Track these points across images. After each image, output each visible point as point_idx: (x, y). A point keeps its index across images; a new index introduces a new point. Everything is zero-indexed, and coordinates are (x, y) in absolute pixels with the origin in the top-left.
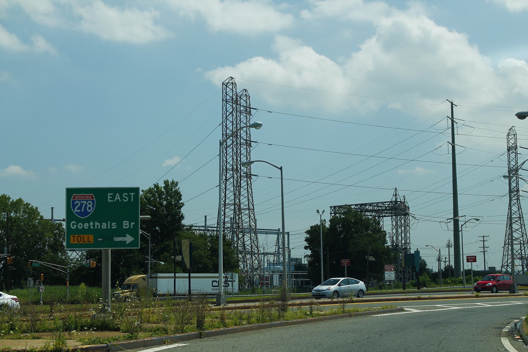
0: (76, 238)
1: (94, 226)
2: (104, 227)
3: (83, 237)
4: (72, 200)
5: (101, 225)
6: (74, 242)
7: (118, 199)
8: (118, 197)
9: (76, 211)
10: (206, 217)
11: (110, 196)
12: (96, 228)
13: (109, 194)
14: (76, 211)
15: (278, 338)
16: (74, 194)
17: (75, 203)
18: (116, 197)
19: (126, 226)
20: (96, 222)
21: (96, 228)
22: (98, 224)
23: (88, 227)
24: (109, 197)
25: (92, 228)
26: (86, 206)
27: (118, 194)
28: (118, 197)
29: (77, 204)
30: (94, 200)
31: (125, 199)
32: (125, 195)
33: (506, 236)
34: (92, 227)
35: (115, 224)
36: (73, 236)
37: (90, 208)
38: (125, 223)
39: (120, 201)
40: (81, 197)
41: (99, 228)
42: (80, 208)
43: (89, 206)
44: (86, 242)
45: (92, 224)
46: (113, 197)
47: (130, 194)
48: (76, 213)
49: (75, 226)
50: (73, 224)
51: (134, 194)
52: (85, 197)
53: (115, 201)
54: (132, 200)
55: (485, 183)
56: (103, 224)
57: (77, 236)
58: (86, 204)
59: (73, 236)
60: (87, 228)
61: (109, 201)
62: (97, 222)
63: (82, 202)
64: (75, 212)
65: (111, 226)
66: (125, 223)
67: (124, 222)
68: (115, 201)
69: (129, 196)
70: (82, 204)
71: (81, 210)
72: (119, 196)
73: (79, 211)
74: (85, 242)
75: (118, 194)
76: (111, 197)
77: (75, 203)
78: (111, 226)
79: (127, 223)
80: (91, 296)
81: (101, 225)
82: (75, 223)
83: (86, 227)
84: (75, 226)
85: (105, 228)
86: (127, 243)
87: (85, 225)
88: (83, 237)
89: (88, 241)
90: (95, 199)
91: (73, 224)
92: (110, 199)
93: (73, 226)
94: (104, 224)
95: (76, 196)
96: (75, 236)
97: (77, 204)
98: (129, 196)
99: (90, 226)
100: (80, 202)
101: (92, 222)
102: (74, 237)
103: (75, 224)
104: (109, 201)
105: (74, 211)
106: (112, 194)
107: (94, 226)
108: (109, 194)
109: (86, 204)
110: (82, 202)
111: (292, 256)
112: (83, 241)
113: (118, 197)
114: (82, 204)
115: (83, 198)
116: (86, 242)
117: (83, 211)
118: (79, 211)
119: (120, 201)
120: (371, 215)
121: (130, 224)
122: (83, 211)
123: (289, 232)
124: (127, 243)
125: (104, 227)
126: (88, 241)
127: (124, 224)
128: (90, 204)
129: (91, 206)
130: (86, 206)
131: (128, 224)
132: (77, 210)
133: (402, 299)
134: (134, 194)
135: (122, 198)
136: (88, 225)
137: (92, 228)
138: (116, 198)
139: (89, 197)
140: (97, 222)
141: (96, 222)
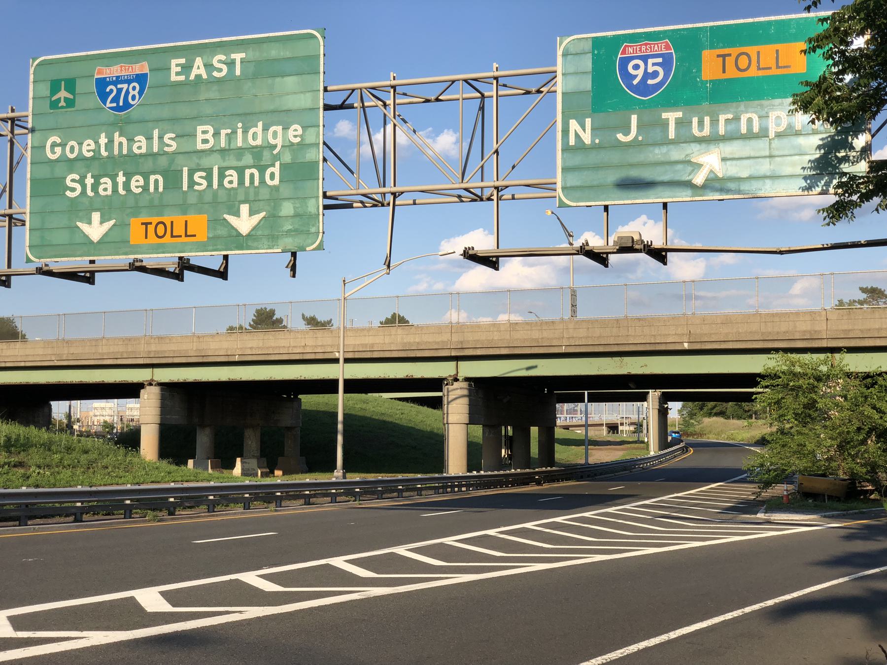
0: (730, 61)
3: (758, 53)
4: (619, 56)
5: (131, 140)
6: (724, 71)
8: (198, 68)
9: (109, 105)
11: (177, 65)
12: (116, 152)
13: (174, 62)
15: (832, 421)
17: (108, 90)
19: (205, 141)
20: (117, 134)
22: (124, 140)
25: (104, 153)
26: (127, 92)
28: (198, 68)
29: (112, 91)
30: (672, 53)
35: (173, 135)
36: (718, 56)
37: (134, 98)
39: (205, 76)
40: (641, 48)
41: (125, 152)
42: (116, 99)
43: (132, 93)
44: (770, 68)
46: (186, 68)
52: (651, 48)
53: (192, 77)
57: (734, 51)
58: (128, 89)
59: (718, 56)
62: (120, 136)
64: (108, 108)
67: (200, 129)
68: (192, 77)
69: (231, 64)
70: (119, 91)
71: (118, 103)
72: (202, 67)
73: (114, 105)
74: (763, 69)
76: (179, 69)
81: (131, 140)
82: (58, 141)
84: (58, 150)
87: (85, 148)
88: (758, 53)
89: (778, 67)
91: (54, 145)
92: (177, 74)
93: (53, 152)
96: (730, 55)
97: (112, 91)
98: (231, 64)
102: (724, 56)
103: (59, 145)
105: (106, 106)
106: (183, 61)
108: (174, 62)
109: (128, 89)
110: (119, 86)
112: (759, 68)
114: (119, 91)
115: (646, 49)
116: (770, 68)
117: (121, 104)
118: (114, 105)
119: (205, 76)
121: (216, 134)
122: (121, 104)
123: (514, 194)
126: (778, 67)
127: (200, 137)
128: (134, 88)
129: (136, 93)
130: (127, 92)
131: (209, 136)
133: (417, 509)
135: (209, 66)
137: (104, 153)
138: (195, 72)
139: (658, 47)
140: (120, 136)
141: (117, 134)
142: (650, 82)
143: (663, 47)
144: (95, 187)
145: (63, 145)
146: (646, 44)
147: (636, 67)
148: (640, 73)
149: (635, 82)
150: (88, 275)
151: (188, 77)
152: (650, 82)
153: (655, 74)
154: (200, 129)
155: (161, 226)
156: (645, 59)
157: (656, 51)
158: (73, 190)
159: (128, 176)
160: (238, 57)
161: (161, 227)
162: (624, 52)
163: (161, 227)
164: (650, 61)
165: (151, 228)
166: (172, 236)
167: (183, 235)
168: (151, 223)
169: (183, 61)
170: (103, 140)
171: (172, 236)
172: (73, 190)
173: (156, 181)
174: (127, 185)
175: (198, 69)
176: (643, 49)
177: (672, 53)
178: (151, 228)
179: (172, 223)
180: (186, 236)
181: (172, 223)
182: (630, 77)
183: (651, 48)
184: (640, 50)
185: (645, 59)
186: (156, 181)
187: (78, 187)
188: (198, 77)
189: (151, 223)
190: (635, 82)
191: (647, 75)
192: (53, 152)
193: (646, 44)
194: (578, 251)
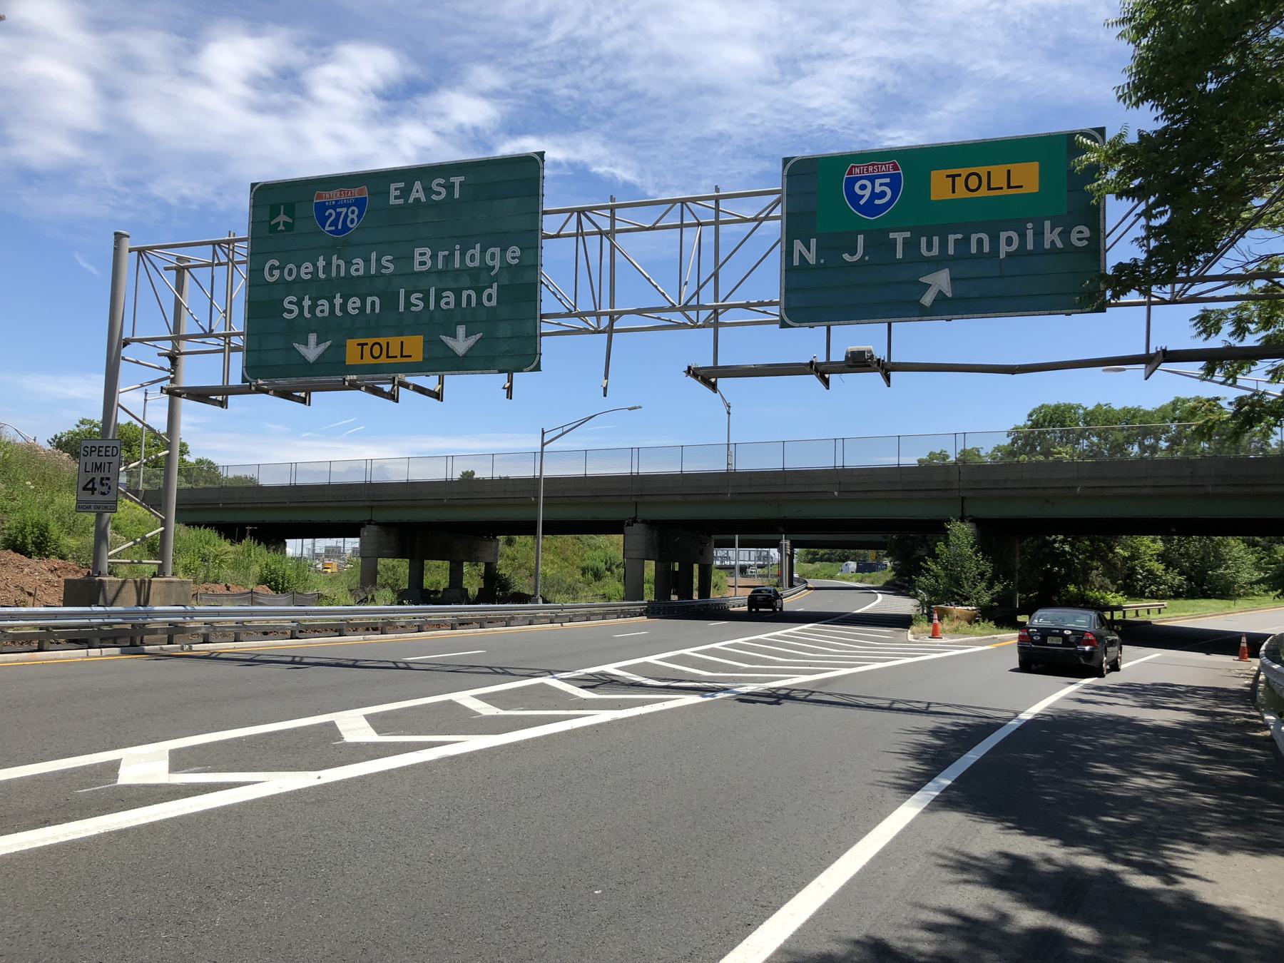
4: (846, 176)
5: (349, 263)
7: (417, 195)
8: (417, 192)
11: (396, 189)
13: (393, 186)
14: (326, 229)
16: (895, 161)
17: (327, 214)
18: (414, 190)
23: (1086, 239)
24: (393, 193)
25: (322, 276)
26: (346, 215)
27: (418, 185)
28: (417, 192)
29: (331, 214)
30: (900, 173)
34: (323, 274)
38: (421, 254)
39: (423, 199)
40: (868, 169)
41: (342, 274)
42: (335, 223)
43: (351, 216)
46: (405, 192)
47: (452, 180)
49: (277, 273)
50: (272, 268)
51: (462, 178)
52: (878, 168)
53: (411, 201)
54: (457, 196)
60: (1085, 243)
61: (392, 201)
63: (338, 210)
66: (421, 254)
67: (417, 251)
68: (411, 201)
69: (450, 187)
70: (339, 214)
71: (337, 227)
72: (421, 190)
73: (333, 228)
76: (398, 193)
79: (425, 254)
80: (1050, 429)
82: (277, 263)
84: (277, 273)
85: (361, 272)
87: (303, 270)
90: (901, 171)
91: (272, 268)
92: (396, 198)
95: (855, 167)
97: (331, 214)
98: (450, 187)
100: (335, 211)
104: (392, 201)
106: (402, 185)
108: (393, 186)
109: (347, 213)
110: (338, 210)
111: (118, 422)
113: (418, 192)
114: (339, 214)
115: (873, 169)
117: (340, 227)
118: (333, 228)
119: (423, 199)
120: (1208, 171)
121: (434, 257)
122: (340, 227)
127: (417, 259)
128: (353, 212)
130: (346, 215)
131: (427, 258)
132: (864, 195)
135: (428, 190)
137: (322, 276)
139: (886, 167)
142: (877, 202)
143: (891, 167)
145: (281, 268)
146: (873, 165)
147: (863, 187)
148: (867, 193)
149: (862, 202)
151: (406, 201)
152: (877, 202)
153: (883, 194)
154: (417, 251)
156: (872, 179)
157: (884, 171)
160: (457, 180)
162: (850, 173)
164: (878, 182)
169: (402, 185)
172: (291, 312)
174: (344, 307)
176: (870, 169)
177: (900, 173)
182: (855, 199)
184: (867, 171)
185: (872, 179)
188: (417, 200)
190: (862, 202)
191: (874, 196)
193: (873, 165)
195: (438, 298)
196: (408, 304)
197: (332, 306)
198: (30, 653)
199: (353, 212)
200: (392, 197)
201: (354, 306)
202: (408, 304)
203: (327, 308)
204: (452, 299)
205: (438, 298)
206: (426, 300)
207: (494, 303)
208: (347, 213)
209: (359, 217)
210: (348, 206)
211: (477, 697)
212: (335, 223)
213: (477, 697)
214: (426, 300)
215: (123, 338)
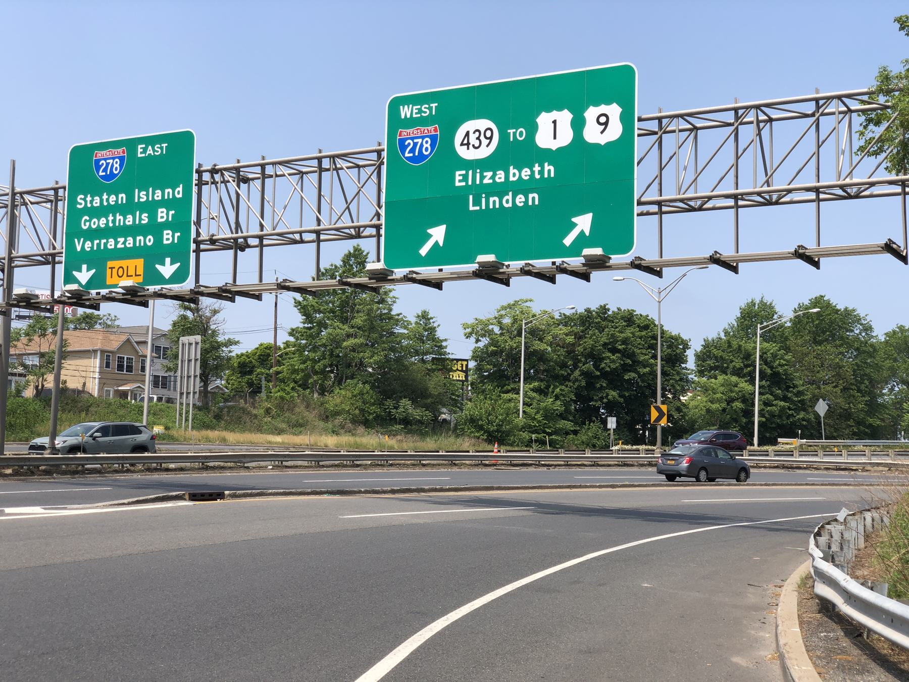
1: (541, 172)
2: (500, 178)
5: (125, 219)
7: (150, 152)
9: (407, 155)
10: (555, 138)
11: (460, 175)
12: (546, 176)
13: (458, 173)
14: (407, 155)
20: (546, 164)
21: (546, 176)
22: (121, 218)
23: (529, 175)
25: (537, 176)
27: (150, 147)
31: (158, 152)
32: (158, 147)
33: (758, 107)
39: (153, 154)
45: (111, 218)
47: (431, 105)
48: (407, 158)
52: (421, 131)
54: (164, 153)
55: (676, 282)
56: (498, 173)
62: (120, 215)
65: (140, 219)
67: (160, 210)
70: (108, 164)
73: (411, 155)
75: (150, 147)
76: (417, 111)
77: (406, 144)
78: (140, 219)
83: (526, 176)
86: (587, 233)
87: (101, 222)
90: (438, 133)
91: (86, 221)
92: (460, 181)
93: (85, 225)
94: (130, 218)
98: (430, 109)
99: (533, 172)
101: (111, 215)
105: (404, 155)
106: (144, 146)
107: (541, 172)
109: (113, 164)
114: (108, 164)
119: (153, 154)
124: (587, 233)
125: (500, 178)
128: (117, 163)
130: (422, 145)
134: (436, 104)
135: (154, 151)
136: (529, 173)
138: (148, 152)
140: (120, 215)
141: (546, 164)
144: (91, 202)
145: (90, 221)
146: (417, 129)
150: (48, 307)
154: (160, 210)
155: (121, 269)
158: (81, 204)
159: (109, 195)
161: (120, 274)
163: (120, 274)
165: (115, 271)
166: (128, 276)
167: (134, 275)
168: (114, 268)
169: (144, 146)
170: (537, 168)
171: (128, 276)
172: (81, 204)
173: (122, 198)
174: (108, 200)
175: (150, 151)
178: (115, 271)
179: (128, 267)
180: (136, 275)
181: (128, 267)
183: (421, 131)
186: (122, 198)
187: (83, 202)
188: (150, 154)
189: (114, 268)
192: (85, 225)
194: (882, 248)
195: (153, 194)
196: (139, 197)
197: (102, 201)
198: (337, 497)
199: (117, 163)
200: (139, 153)
201: (521, 200)
202: (139, 197)
203: (98, 201)
204: (131, 241)
205: (153, 194)
206: (147, 195)
207: (180, 196)
208: (113, 164)
209: (121, 166)
210: (114, 159)
211: (55, 241)
212: (105, 170)
213: (55, 241)
214: (147, 195)
215: (201, 298)
